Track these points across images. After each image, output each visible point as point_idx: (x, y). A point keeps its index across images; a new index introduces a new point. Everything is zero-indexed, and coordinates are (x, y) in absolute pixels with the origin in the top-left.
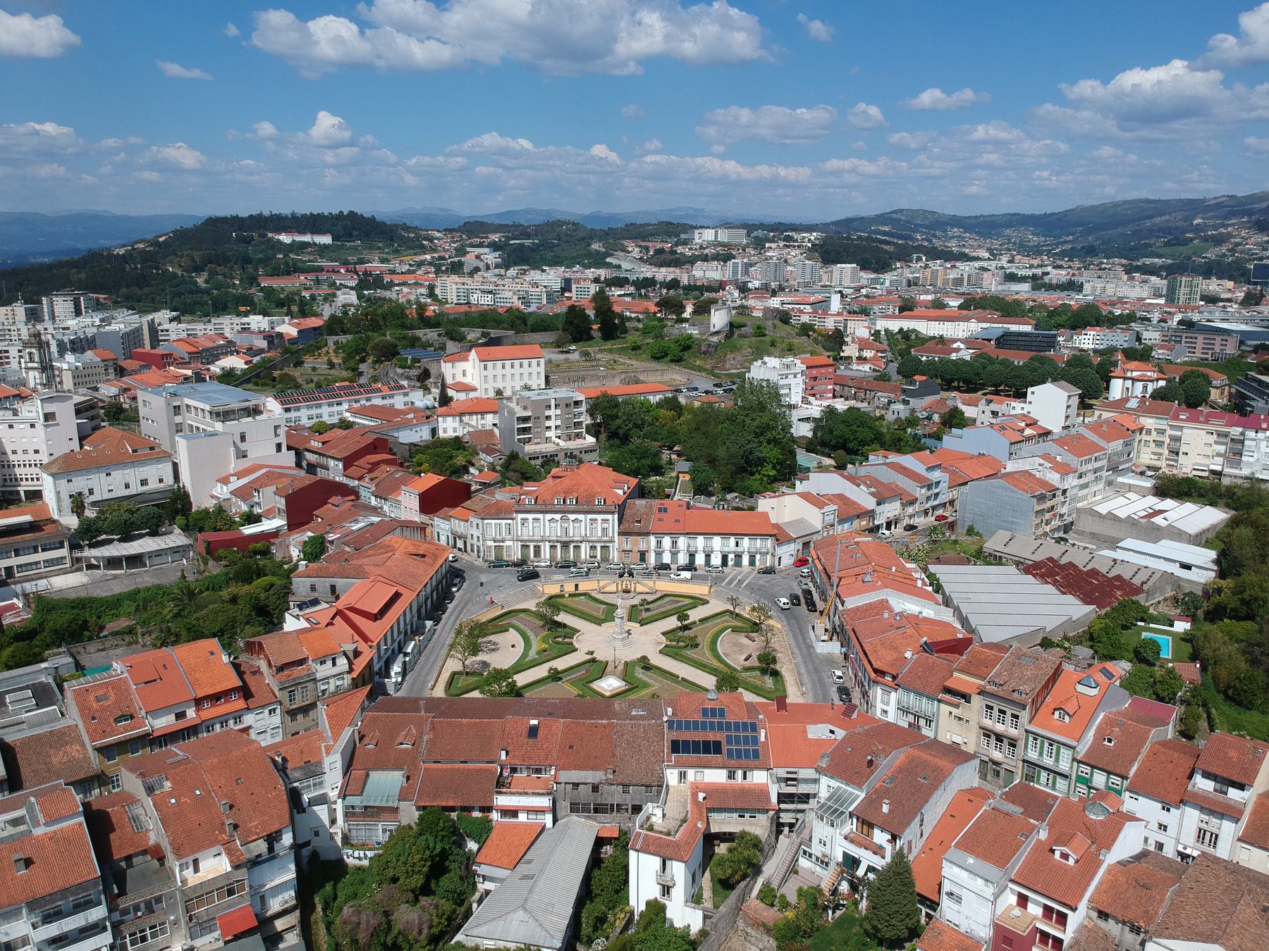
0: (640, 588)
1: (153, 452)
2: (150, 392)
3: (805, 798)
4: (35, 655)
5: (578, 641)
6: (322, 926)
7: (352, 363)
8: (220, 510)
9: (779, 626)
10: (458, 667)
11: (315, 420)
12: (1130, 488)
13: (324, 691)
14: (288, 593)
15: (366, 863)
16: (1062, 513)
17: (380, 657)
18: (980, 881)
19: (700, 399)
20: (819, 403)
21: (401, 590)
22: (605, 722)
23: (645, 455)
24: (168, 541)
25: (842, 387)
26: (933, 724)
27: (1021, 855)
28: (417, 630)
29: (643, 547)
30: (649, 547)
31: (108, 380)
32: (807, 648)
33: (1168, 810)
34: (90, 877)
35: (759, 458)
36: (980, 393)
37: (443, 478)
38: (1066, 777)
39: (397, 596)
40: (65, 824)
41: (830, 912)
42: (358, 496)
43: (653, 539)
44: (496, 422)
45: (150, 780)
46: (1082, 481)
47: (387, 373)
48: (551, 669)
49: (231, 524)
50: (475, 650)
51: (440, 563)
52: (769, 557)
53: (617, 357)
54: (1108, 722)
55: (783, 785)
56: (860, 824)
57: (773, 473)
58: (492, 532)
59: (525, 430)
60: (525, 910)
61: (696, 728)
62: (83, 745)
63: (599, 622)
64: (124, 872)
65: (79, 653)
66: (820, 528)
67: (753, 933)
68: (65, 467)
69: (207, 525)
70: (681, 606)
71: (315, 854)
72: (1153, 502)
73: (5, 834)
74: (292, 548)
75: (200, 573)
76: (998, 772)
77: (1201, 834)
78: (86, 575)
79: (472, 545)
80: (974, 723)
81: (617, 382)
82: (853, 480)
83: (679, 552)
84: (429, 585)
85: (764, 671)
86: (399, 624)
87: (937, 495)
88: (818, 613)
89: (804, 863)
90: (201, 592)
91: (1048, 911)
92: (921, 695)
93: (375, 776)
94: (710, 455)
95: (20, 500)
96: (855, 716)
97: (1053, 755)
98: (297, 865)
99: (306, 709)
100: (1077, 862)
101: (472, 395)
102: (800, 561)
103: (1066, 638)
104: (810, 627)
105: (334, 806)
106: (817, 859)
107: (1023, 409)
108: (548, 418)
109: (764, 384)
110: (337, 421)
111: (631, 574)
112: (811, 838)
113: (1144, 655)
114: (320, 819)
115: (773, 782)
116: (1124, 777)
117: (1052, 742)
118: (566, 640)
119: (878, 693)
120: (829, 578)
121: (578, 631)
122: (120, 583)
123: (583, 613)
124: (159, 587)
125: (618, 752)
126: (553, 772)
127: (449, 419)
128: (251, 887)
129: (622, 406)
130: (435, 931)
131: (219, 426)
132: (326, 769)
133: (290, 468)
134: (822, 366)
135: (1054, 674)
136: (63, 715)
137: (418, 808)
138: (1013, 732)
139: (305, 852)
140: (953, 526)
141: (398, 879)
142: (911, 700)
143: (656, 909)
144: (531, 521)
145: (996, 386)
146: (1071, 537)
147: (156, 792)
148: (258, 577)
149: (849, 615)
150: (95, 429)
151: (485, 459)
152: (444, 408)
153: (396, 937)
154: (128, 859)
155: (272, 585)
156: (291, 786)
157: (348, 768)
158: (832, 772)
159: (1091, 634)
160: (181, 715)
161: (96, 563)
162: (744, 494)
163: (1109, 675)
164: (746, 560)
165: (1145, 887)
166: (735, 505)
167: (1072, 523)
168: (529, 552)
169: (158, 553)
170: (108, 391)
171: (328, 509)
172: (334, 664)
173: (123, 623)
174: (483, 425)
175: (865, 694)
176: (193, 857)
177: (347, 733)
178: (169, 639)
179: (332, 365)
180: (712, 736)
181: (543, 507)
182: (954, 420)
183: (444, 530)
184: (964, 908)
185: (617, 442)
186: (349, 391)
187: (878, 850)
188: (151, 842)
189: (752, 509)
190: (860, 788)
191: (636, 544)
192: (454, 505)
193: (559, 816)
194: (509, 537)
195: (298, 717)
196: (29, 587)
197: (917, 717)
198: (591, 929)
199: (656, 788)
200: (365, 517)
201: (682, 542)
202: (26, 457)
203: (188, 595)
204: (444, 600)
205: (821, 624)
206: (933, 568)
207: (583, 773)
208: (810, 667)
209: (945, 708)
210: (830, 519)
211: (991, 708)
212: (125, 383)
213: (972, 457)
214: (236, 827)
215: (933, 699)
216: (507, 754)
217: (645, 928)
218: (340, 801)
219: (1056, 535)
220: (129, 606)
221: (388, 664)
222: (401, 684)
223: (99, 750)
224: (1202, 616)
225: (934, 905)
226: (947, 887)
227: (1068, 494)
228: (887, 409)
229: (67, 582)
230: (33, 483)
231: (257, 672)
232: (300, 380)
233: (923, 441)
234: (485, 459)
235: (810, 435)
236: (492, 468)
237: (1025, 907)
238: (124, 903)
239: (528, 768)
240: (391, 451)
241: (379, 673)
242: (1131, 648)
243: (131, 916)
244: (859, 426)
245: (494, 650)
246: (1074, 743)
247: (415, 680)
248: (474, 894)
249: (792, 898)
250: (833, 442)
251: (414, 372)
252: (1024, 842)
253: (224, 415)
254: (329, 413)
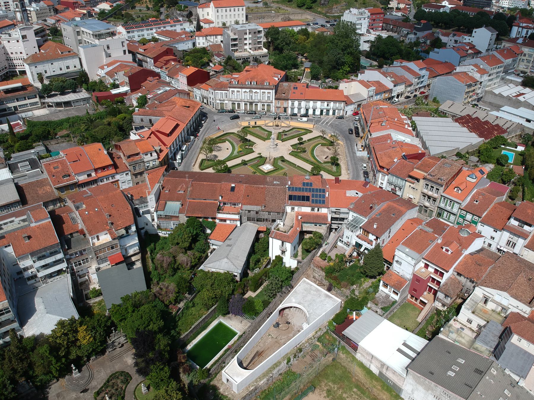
0: (283, 125)
1: (71, 54)
2: (66, 24)
3: (343, 219)
4: (29, 146)
5: (255, 148)
6: (150, 260)
7: (157, 8)
8: (101, 82)
9: (342, 143)
10: (204, 157)
11: (141, 37)
12: (511, 81)
13: (148, 166)
14: (132, 122)
15: (167, 235)
16: (478, 93)
17: (171, 152)
18: (410, 258)
19: (318, 29)
20: (374, 33)
21: (179, 123)
22: (262, 186)
23: (290, 59)
24: (80, 95)
25: (387, 25)
26: (402, 190)
27: (429, 248)
28: (187, 140)
29: (285, 106)
30: (288, 106)
31: (51, 15)
32: (352, 153)
33: (496, 232)
34: (55, 243)
35: (343, 62)
36: (451, 30)
37: (197, 69)
38: (455, 215)
39: (177, 126)
40: (43, 222)
41: (348, 263)
42: (160, 78)
43: (290, 102)
44: (222, 40)
45: (77, 204)
46: (490, 78)
47: (173, 13)
48: (243, 160)
49: (106, 89)
50: (211, 151)
51: (196, 111)
52: (341, 111)
53: (280, 6)
54: (478, 193)
55: (334, 214)
56: (364, 232)
57: (348, 69)
58: (219, 97)
59: (235, 45)
60: (227, 258)
61: (300, 190)
62: (51, 186)
63: (264, 139)
64: (70, 239)
65: (48, 145)
66: (366, 98)
67: (317, 270)
68: (34, 60)
69: (97, 88)
70: (300, 133)
71: (146, 232)
72: (520, 89)
73: (19, 226)
74: (133, 101)
75: (95, 110)
76: (427, 211)
77: (508, 243)
78: (48, 110)
79: (210, 102)
80: (419, 191)
81: (279, 19)
82: (385, 74)
83: (301, 108)
84: (191, 121)
85: (333, 164)
86: (179, 138)
87: (422, 82)
88: (360, 138)
89: (339, 244)
90: (96, 120)
91: (436, 271)
92: (398, 178)
93: (169, 203)
94: (320, 60)
95: (17, 75)
96: (368, 186)
97: (451, 206)
98: (138, 238)
99: (141, 174)
100: (452, 253)
101: (212, 25)
102: (356, 113)
103: (468, 153)
104: (355, 145)
105: (153, 215)
106: (345, 243)
107: (469, 39)
108: (246, 39)
109: (349, 24)
110: (151, 38)
111: (279, 118)
112: (343, 235)
113: (500, 162)
114: (148, 219)
115: (330, 213)
116: (479, 217)
117: (451, 201)
118: (250, 147)
119: (380, 176)
120: (367, 123)
121: (255, 143)
122: (62, 114)
123: (258, 135)
124: (78, 117)
125: (267, 198)
126: (240, 206)
127: (201, 38)
128: (120, 246)
129: (281, 34)
130: (193, 264)
131: (97, 42)
132: (149, 200)
133: (130, 62)
134: (378, 14)
135: (458, 172)
136: (42, 172)
137: (187, 217)
138: (435, 195)
139: (143, 231)
140: (427, 97)
141: (179, 243)
142: (394, 179)
143: (279, 259)
144: (236, 92)
145: (459, 27)
146: (480, 104)
147: (80, 209)
148: (119, 114)
149: (372, 140)
150: (46, 41)
151: (217, 59)
152: (199, 32)
153: (178, 266)
154: (71, 234)
155: (125, 118)
156: (135, 207)
157: (158, 200)
158: (354, 210)
159: (479, 151)
160: (89, 175)
161: (51, 104)
162: (334, 80)
163: (482, 172)
164: (331, 112)
165: (479, 265)
166: (329, 85)
167: (482, 97)
168: (235, 106)
169: (77, 101)
170: (51, 21)
171: (147, 83)
172: (151, 155)
173: (65, 132)
174: (216, 41)
175: (375, 175)
176: (96, 235)
177: (157, 186)
178: (83, 141)
179: (148, 9)
180: (306, 194)
181: (241, 85)
182: (437, 44)
183: (198, 94)
184: (402, 267)
185: (277, 52)
186: (156, 23)
187: (370, 242)
188: (80, 228)
189: (337, 88)
190: (366, 218)
191: (282, 104)
192: (202, 82)
193: (243, 222)
194: (226, 99)
195: (138, 176)
196: (23, 115)
197: (395, 186)
198: (253, 265)
199: (282, 213)
200: (163, 87)
201: (303, 103)
202: (17, 55)
203: (90, 121)
204: (199, 127)
205: (360, 143)
206: (414, 118)
207: (253, 207)
208: (353, 162)
209: (408, 184)
210: (371, 93)
211: (428, 185)
212: (58, 17)
213: (442, 63)
214: (112, 224)
215: (403, 180)
216: (222, 198)
217: (274, 266)
218: (155, 213)
219: (473, 103)
220: (66, 125)
221: (175, 154)
222: (181, 163)
223: (58, 189)
224: (531, 144)
225: (391, 264)
226: (396, 258)
227: (482, 84)
228: (406, 37)
229: (40, 113)
230: (21, 67)
231: (119, 157)
232: (134, 16)
233: (420, 54)
234: (217, 59)
235: (368, 49)
236: (220, 64)
237: (427, 268)
238: (70, 252)
239: (230, 203)
240: (174, 55)
241: (172, 159)
242: (495, 158)
243: (74, 256)
244: (391, 46)
245: (219, 150)
246: (460, 202)
247: (187, 162)
248: (209, 250)
249: (333, 257)
250: (379, 54)
251: (185, 13)
252: (431, 244)
253: (99, 36)
254: (148, 34)
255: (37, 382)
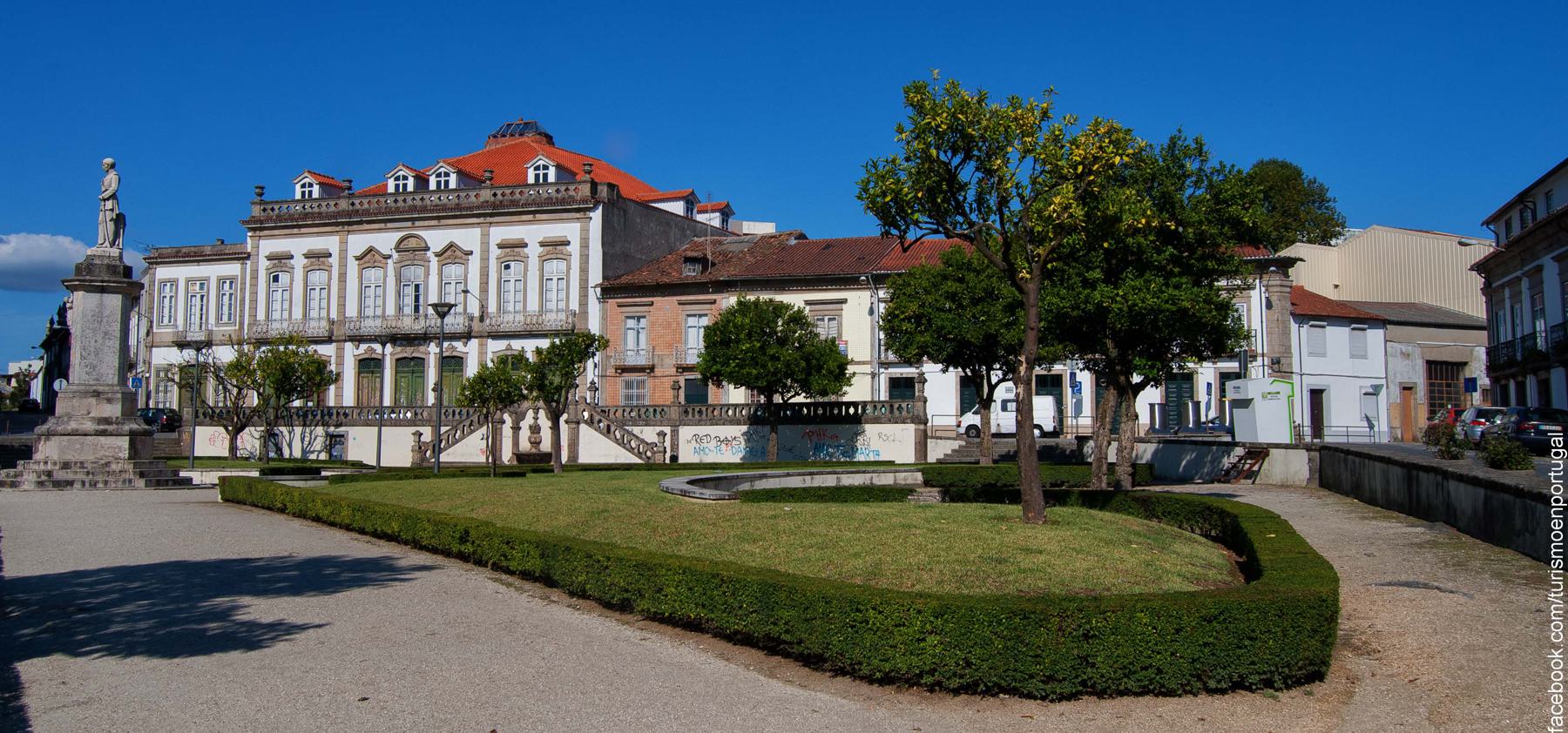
255: (906, 195)
